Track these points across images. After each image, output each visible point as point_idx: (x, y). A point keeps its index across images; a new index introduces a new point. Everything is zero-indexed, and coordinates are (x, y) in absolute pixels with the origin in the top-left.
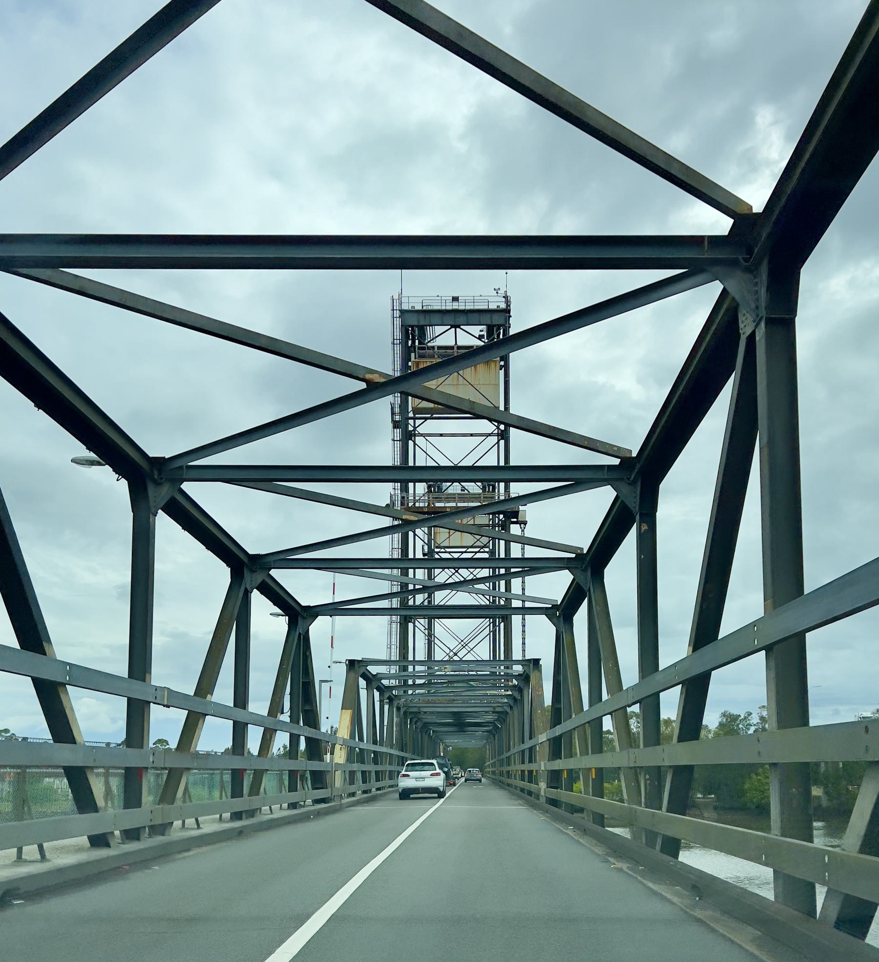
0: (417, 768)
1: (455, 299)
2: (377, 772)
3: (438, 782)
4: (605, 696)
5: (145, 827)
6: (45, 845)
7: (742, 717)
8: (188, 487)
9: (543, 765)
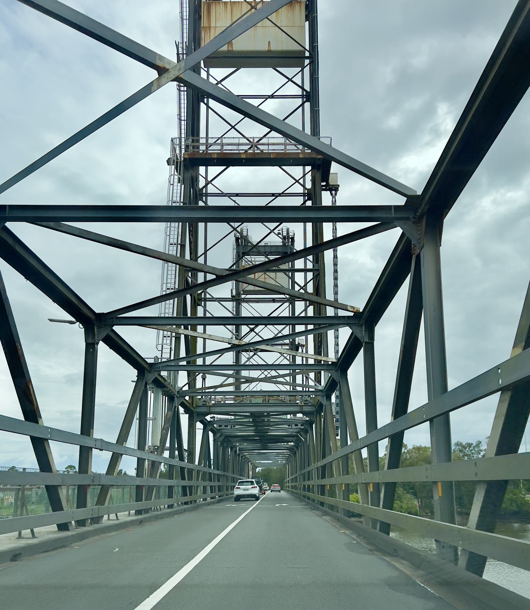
2: (184, 488)
3: (256, 491)
4: (349, 443)
5: (88, 519)
6: (35, 530)
7: (474, 445)
8: (117, 329)
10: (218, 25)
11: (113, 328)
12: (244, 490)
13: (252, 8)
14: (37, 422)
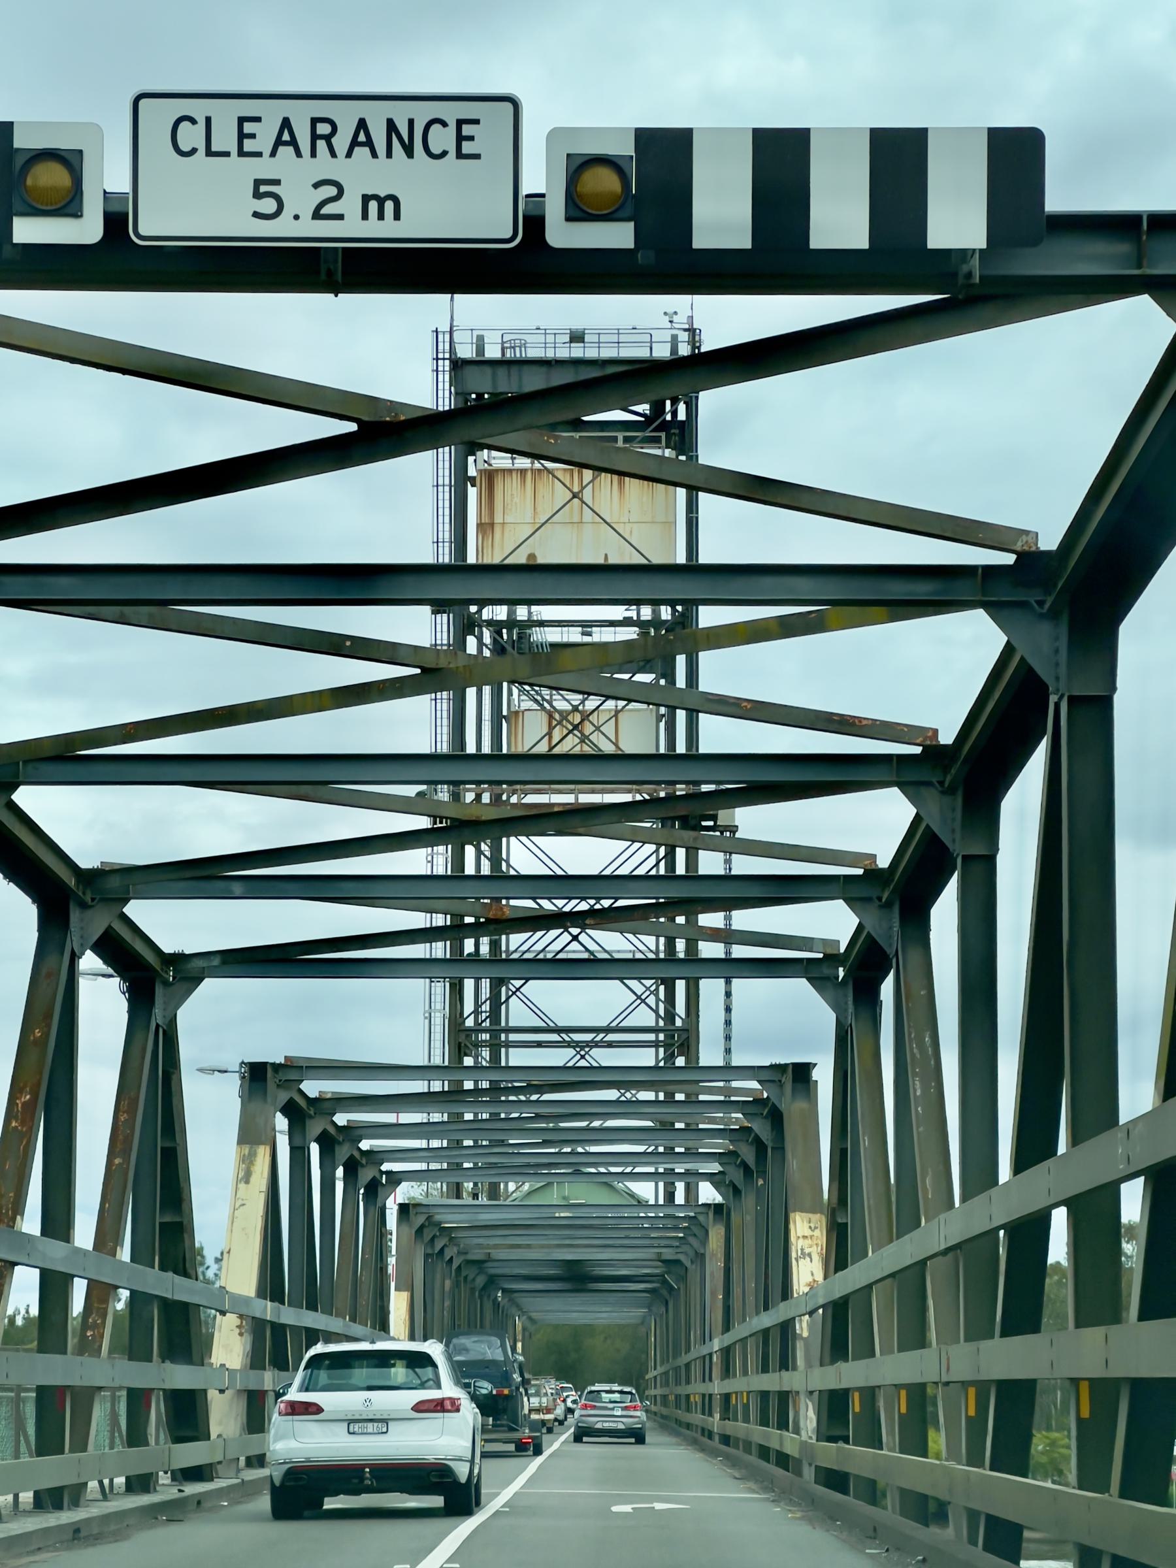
0: (360, 1374)
1: (577, 337)
3: (451, 1439)
9: (809, 1376)
10: (508, 519)
11: (334, 1119)
12: (354, 1423)
13: (575, 496)
14: (68, 1241)
